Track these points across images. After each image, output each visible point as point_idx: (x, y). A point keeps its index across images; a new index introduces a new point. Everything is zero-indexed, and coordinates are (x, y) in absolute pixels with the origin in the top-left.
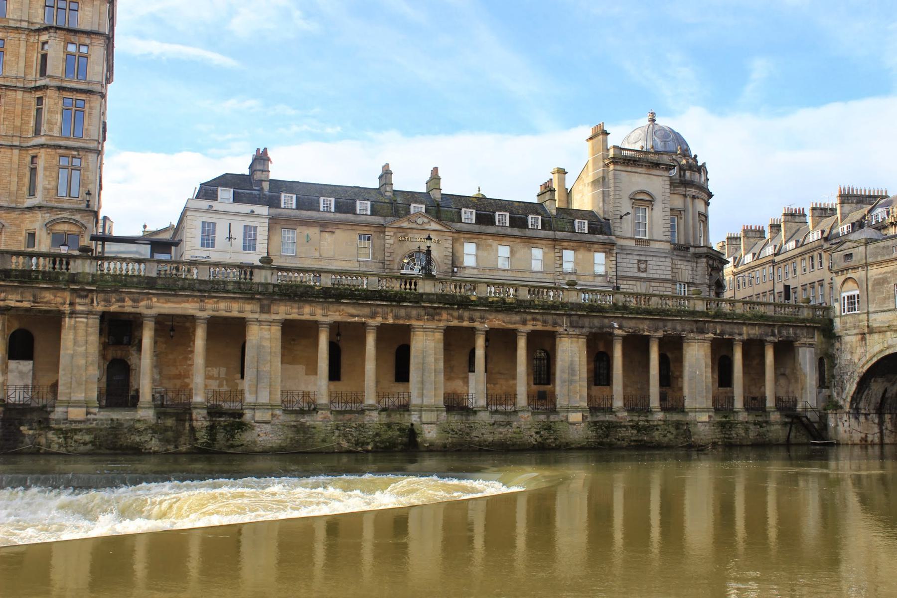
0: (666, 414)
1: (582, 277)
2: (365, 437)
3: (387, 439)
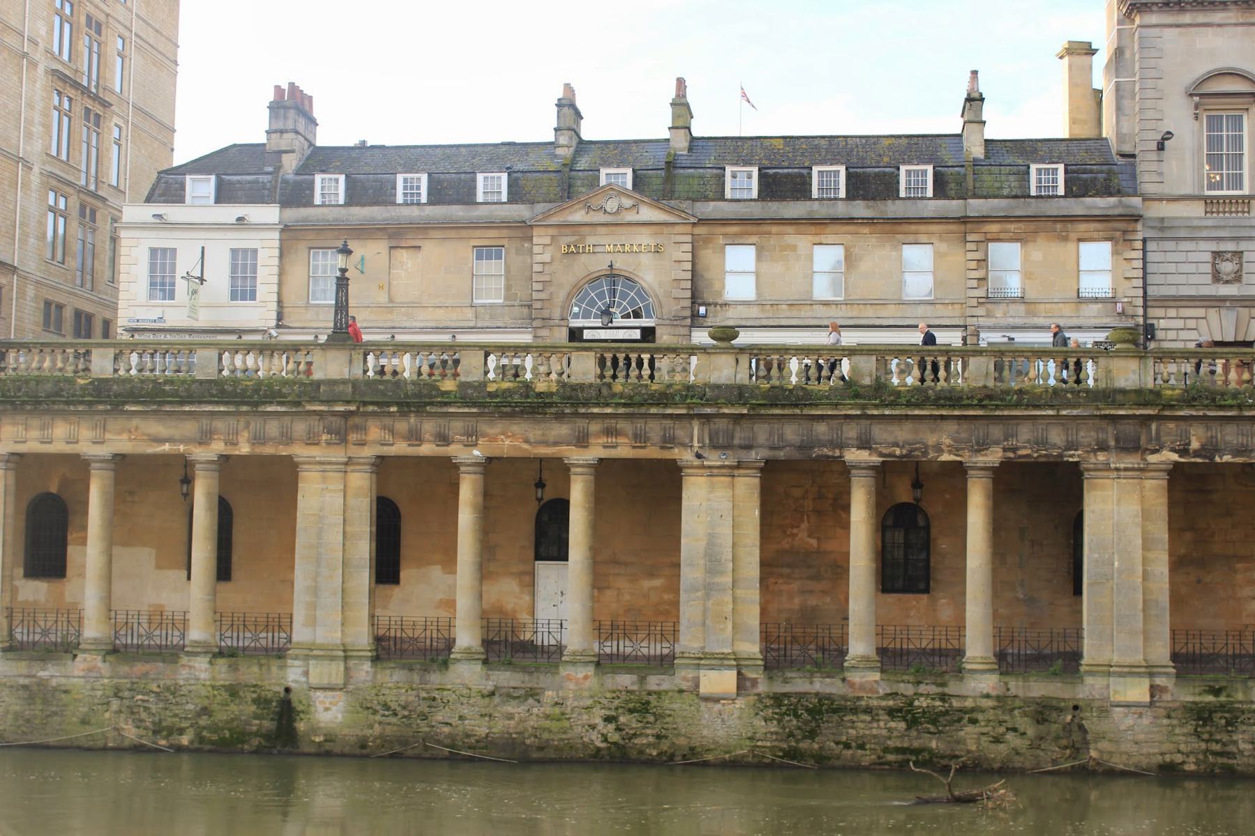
0: (1007, 679)
2: (176, 715)
3: (227, 722)
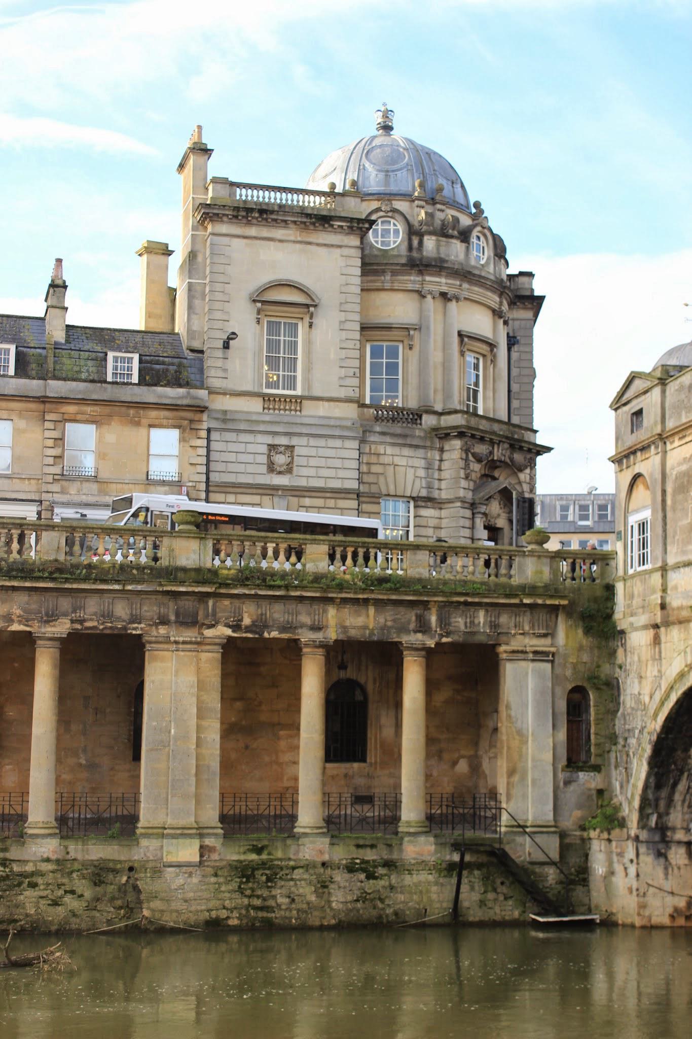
0: (66, 843)
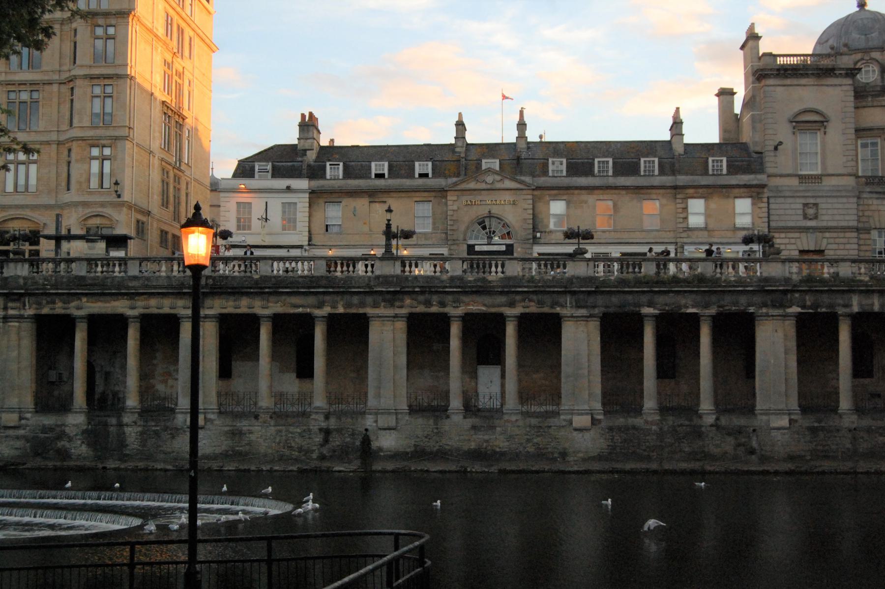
1: (716, 233)
